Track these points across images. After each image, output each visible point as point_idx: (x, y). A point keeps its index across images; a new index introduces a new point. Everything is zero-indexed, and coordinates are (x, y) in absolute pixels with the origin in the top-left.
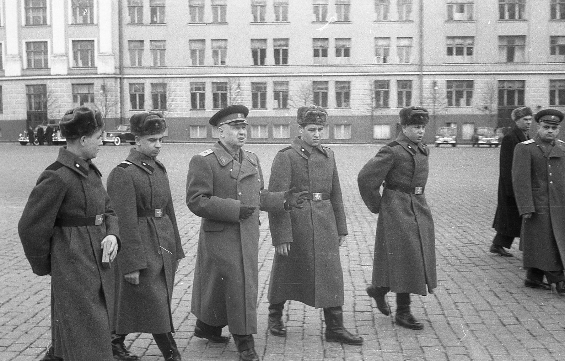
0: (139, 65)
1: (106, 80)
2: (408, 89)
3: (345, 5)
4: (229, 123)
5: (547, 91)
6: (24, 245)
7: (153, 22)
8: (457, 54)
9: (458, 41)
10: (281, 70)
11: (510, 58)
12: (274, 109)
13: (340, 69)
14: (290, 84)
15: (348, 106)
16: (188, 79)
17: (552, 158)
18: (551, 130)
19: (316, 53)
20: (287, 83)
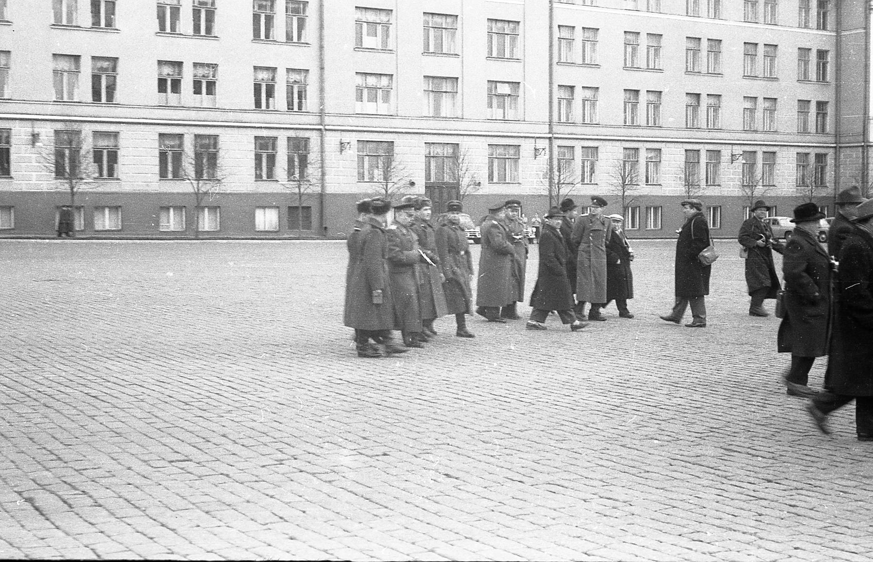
0: (69, 98)
5: (157, 153)
10: (103, 111)
15: (213, 178)
16: (357, 133)
19: (162, 84)
20: (116, 135)
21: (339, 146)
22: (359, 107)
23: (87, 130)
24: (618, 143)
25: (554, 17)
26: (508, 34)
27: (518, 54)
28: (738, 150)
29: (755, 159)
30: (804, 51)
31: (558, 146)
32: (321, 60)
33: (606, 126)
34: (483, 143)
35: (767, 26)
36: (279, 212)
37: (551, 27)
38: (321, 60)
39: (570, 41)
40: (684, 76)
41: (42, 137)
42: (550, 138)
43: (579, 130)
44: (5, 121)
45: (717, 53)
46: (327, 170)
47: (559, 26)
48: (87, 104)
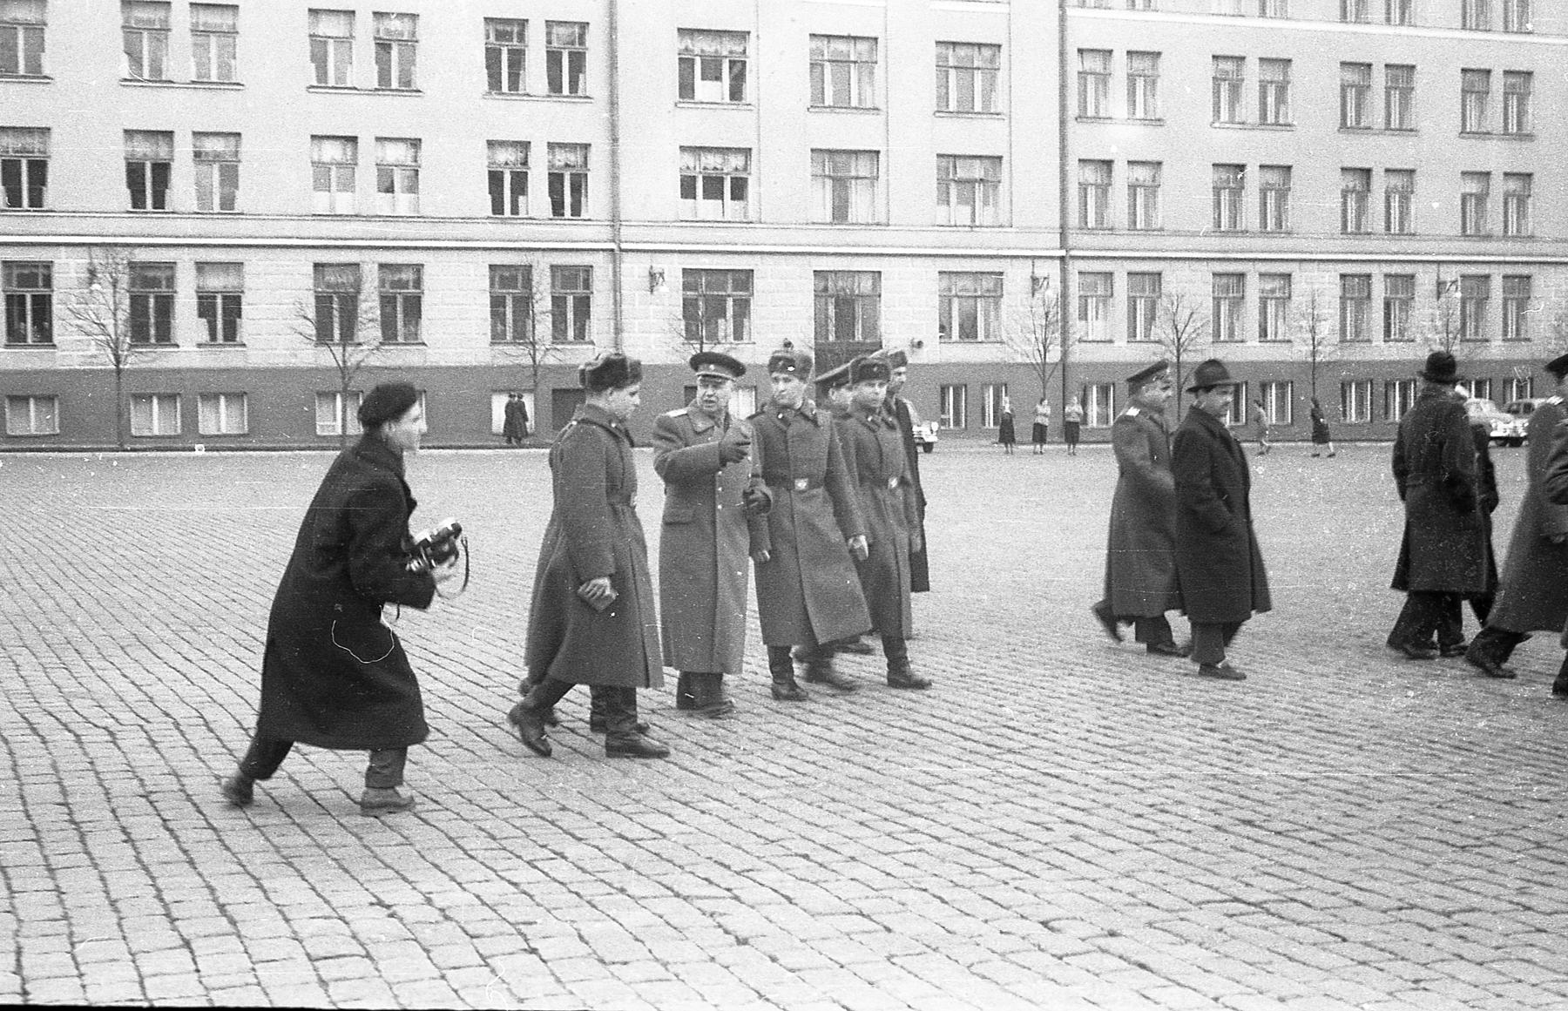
2: (580, 291)
8: (707, 196)
9: (712, 161)
12: (199, 345)
13: (391, 229)
14: (246, 269)
15: (413, 338)
21: (1029, 283)
22: (321, 202)
23: (185, 263)
27: (1000, 104)
28: (1450, 274)
29: (1488, 291)
31: (1080, 273)
32: (613, 127)
33: (1176, 233)
34: (1204, 272)
36: (536, 399)
37: (1062, 54)
38: (613, 127)
39: (1103, 78)
42: (1062, 258)
43: (1122, 243)
44: (564, 254)
45: (1406, 93)
46: (626, 322)
47: (1080, 51)
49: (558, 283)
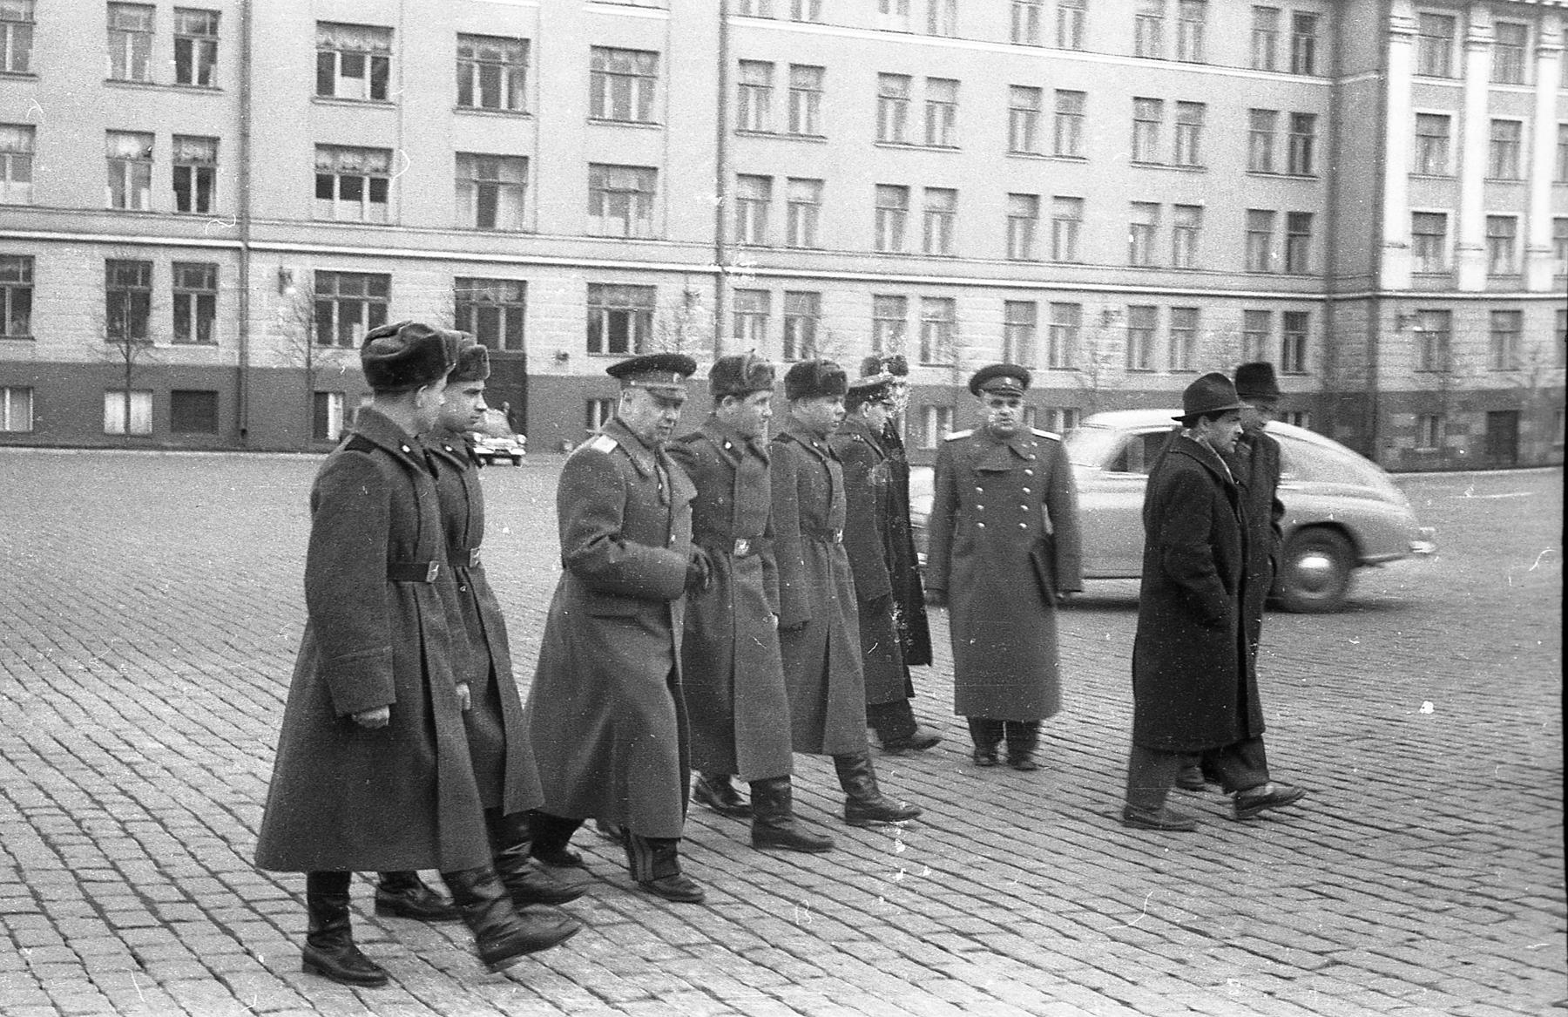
0: (133, 206)
1: (693, 279)
3: (18, 25)
4: (650, 390)
6: (514, 699)
7: (930, 143)
8: (345, 195)
9: (349, 160)
11: (486, 218)
17: (986, 473)
18: (1006, 409)
21: (276, 280)
24: (861, 286)
25: (730, 43)
26: (635, 76)
27: (656, 115)
30: (1262, 117)
35: (1189, 67)
37: (722, 65)
39: (764, 90)
40: (871, 148)
41: (296, 278)
42: (716, 274)
47: (742, 62)
48: (164, 216)
49: (181, 281)
